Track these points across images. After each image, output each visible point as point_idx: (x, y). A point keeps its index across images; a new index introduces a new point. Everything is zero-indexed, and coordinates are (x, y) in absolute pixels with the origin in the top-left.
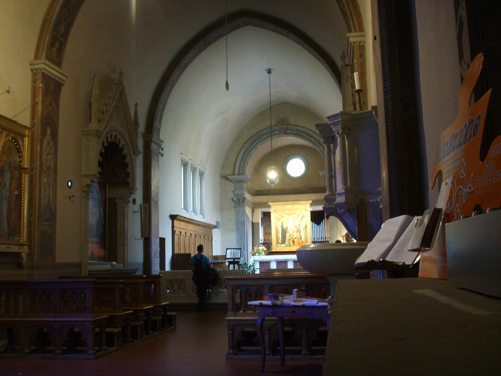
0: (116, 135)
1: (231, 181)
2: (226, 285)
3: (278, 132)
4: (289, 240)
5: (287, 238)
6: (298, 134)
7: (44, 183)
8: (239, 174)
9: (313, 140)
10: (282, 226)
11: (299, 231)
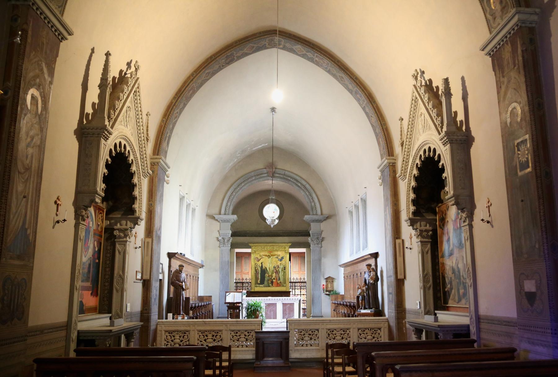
0: (125, 145)
1: (217, 220)
2: (239, 337)
3: (266, 175)
4: (268, 280)
5: (266, 279)
6: (286, 177)
7: (17, 191)
8: (225, 214)
9: (299, 185)
10: (262, 266)
11: (277, 272)
